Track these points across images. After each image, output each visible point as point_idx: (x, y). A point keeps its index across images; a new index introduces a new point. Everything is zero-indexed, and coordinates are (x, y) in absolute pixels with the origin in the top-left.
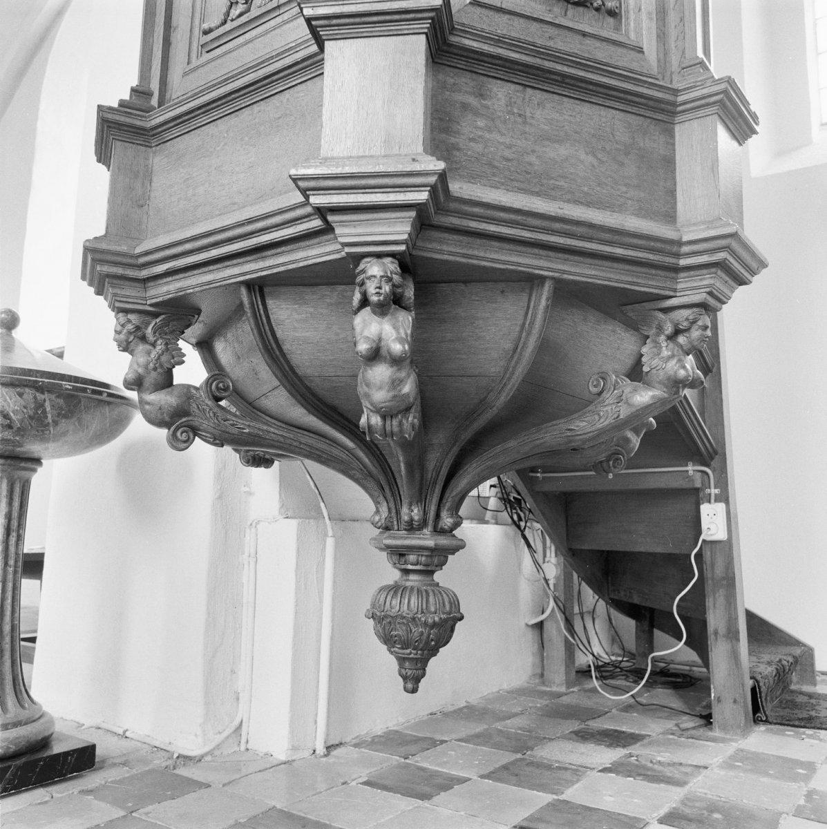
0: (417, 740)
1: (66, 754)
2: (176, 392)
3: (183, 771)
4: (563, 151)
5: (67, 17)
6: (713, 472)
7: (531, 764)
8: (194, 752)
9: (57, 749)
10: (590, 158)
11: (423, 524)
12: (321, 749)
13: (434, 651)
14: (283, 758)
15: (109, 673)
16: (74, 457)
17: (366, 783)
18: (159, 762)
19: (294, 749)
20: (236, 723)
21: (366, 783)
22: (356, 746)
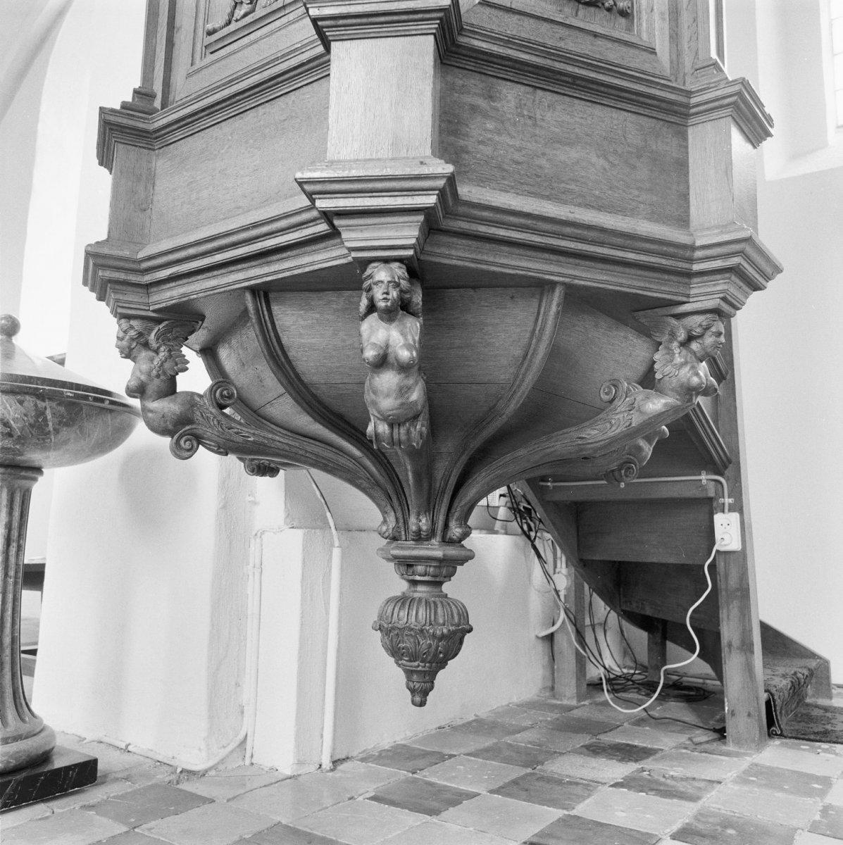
0: (425, 754)
1: (67, 769)
2: (179, 400)
3: (186, 786)
4: (574, 154)
5: (68, 17)
6: (727, 481)
7: (541, 778)
8: (198, 766)
9: (58, 763)
10: (602, 162)
11: (432, 534)
12: (327, 764)
13: (442, 664)
14: (288, 772)
15: (111, 686)
16: (76, 466)
17: (373, 798)
18: (162, 776)
19: (300, 763)
20: (241, 737)
21: (373, 798)
22: (363, 760)
